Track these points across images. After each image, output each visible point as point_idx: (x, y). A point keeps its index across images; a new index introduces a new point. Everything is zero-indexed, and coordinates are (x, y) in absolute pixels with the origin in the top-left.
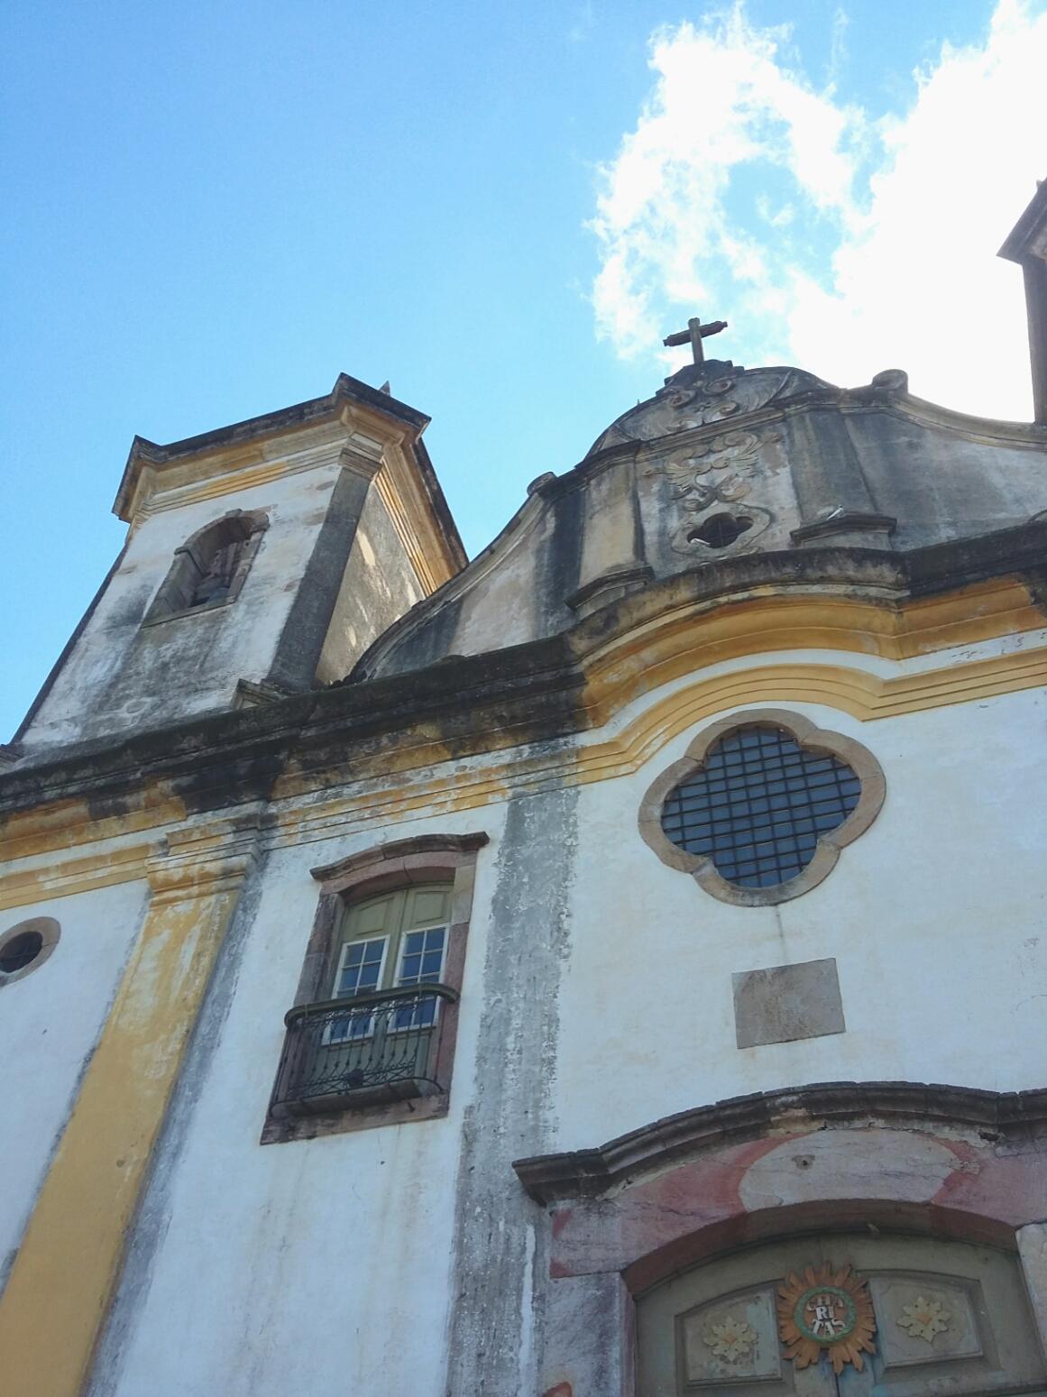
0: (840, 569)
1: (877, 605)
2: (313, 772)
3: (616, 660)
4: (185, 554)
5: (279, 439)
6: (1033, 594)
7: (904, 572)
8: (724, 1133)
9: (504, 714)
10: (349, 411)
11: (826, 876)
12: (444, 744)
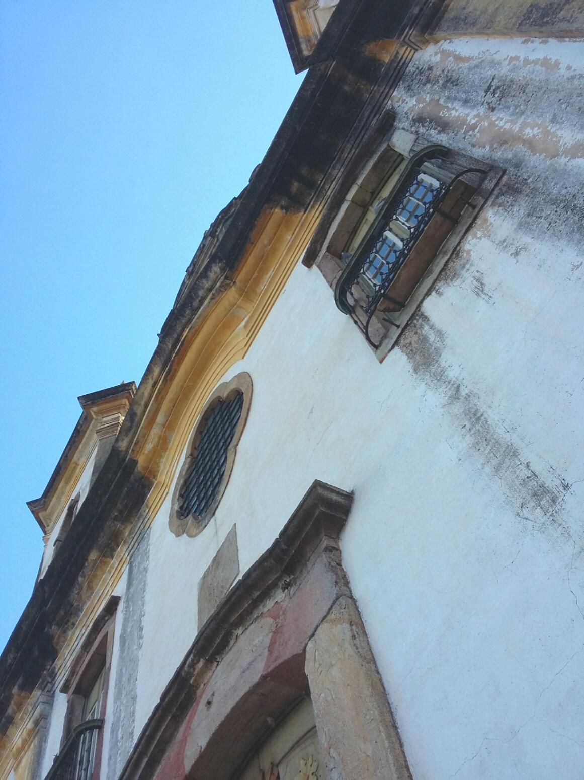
1: (226, 290)
2: (64, 626)
3: (146, 437)
4: (58, 542)
5: (78, 451)
7: (221, 261)
8: (174, 717)
9: (116, 514)
10: (93, 411)
11: (231, 471)
12: (104, 556)
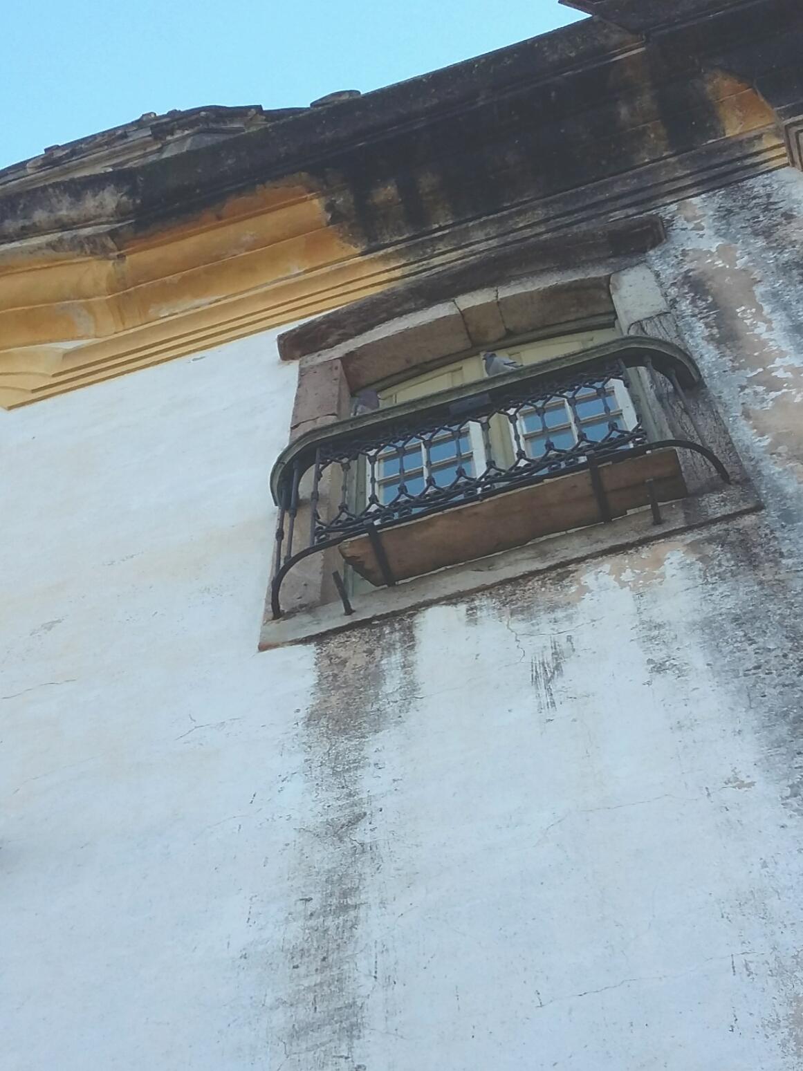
0: (51, 211)
1: (92, 253)
6: (330, 207)
7: (131, 194)
